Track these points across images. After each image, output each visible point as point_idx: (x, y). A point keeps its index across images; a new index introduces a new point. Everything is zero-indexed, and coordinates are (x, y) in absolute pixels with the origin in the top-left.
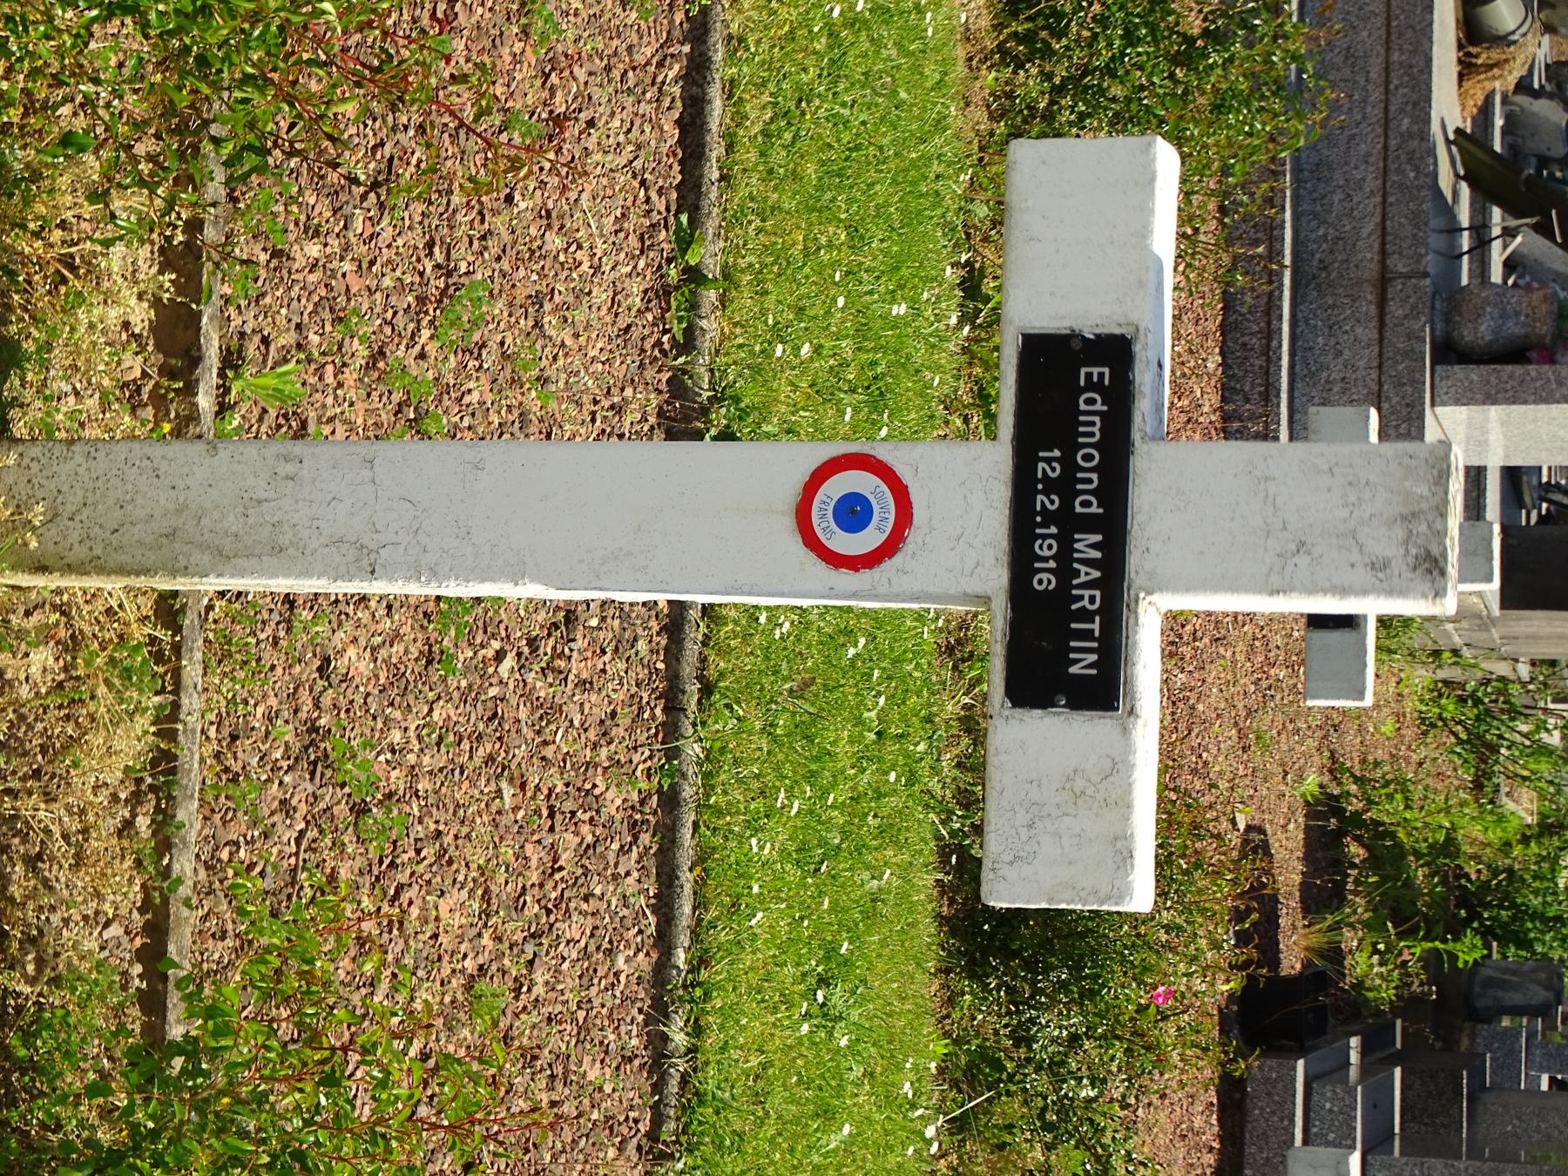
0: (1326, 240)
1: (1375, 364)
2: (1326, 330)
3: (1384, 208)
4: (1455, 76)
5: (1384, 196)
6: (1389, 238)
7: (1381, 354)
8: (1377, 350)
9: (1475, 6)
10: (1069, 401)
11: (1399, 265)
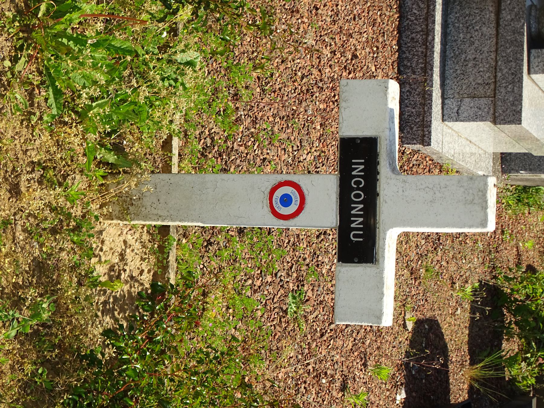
1: (493, 49)
2: (465, 29)
7: (497, 43)
8: (495, 41)
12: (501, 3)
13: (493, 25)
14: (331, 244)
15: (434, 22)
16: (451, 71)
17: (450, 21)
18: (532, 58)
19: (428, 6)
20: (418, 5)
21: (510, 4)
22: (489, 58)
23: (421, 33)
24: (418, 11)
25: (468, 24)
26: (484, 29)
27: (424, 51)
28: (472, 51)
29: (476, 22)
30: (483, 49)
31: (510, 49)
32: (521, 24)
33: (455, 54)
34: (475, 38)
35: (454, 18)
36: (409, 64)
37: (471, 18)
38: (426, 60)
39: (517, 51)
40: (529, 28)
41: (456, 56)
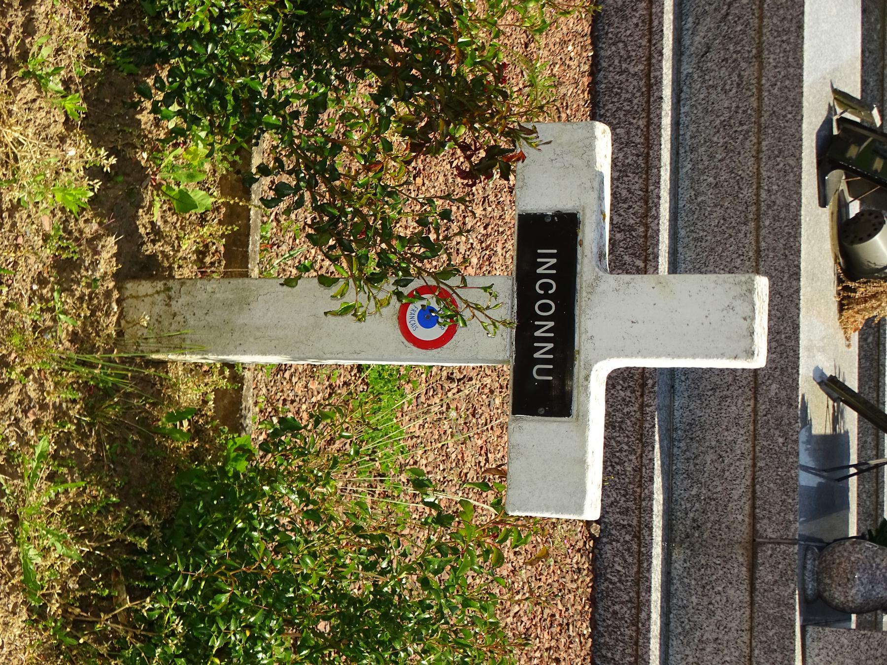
0: (699, 500)
1: (746, 626)
2: (700, 590)
3: (754, 472)
4: (835, 307)
5: (754, 458)
6: (759, 503)
7: (752, 618)
8: (748, 613)
9: (852, 243)
10: (549, 238)
11: (768, 530)
12: (757, 553)
13: (745, 586)
14: (502, 400)
15: (649, 590)
16: (679, 657)
17: (674, 573)
18: (809, 641)
19: (640, 563)
20: (623, 556)
21: (771, 556)
22: (739, 641)
23: (629, 605)
24: (624, 568)
25: (704, 582)
26: (731, 592)
27: (634, 634)
28: (711, 627)
29: (717, 579)
30: (729, 625)
31: (774, 631)
32: (790, 591)
33: (684, 628)
34: (716, 606)
35: (682, 570)
36: (609, 655)
37: (709, 572)
38: (637, 651)
39: (784, 634)
40: (803, 591)
41: (686, 633)
